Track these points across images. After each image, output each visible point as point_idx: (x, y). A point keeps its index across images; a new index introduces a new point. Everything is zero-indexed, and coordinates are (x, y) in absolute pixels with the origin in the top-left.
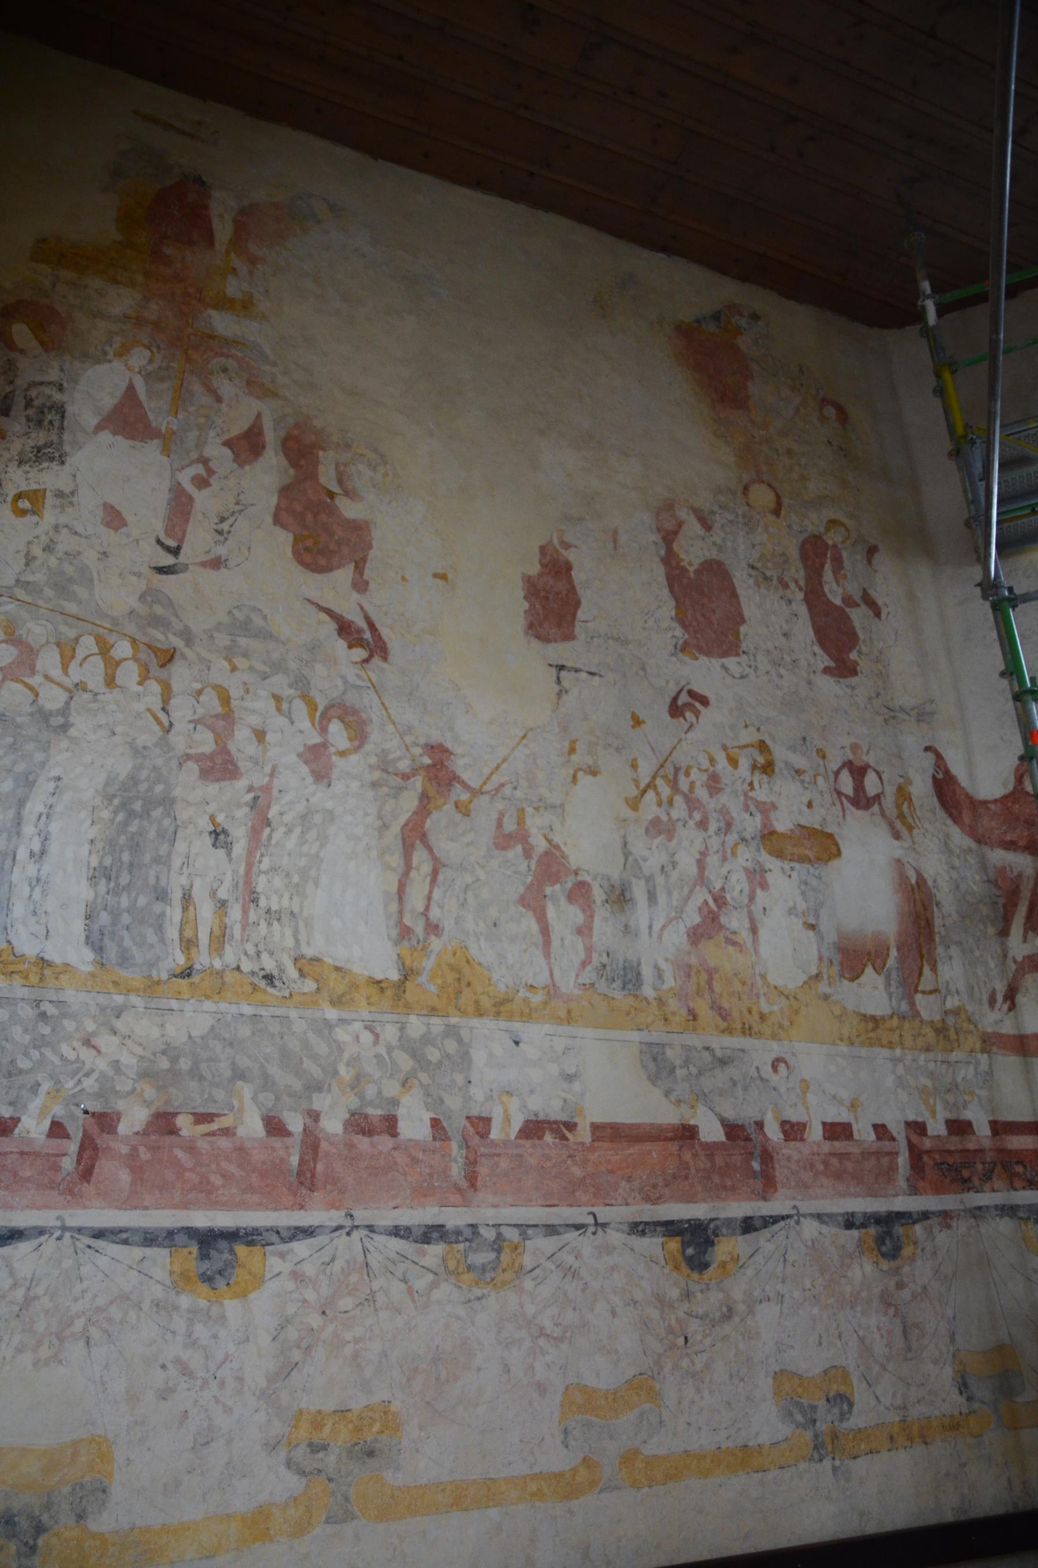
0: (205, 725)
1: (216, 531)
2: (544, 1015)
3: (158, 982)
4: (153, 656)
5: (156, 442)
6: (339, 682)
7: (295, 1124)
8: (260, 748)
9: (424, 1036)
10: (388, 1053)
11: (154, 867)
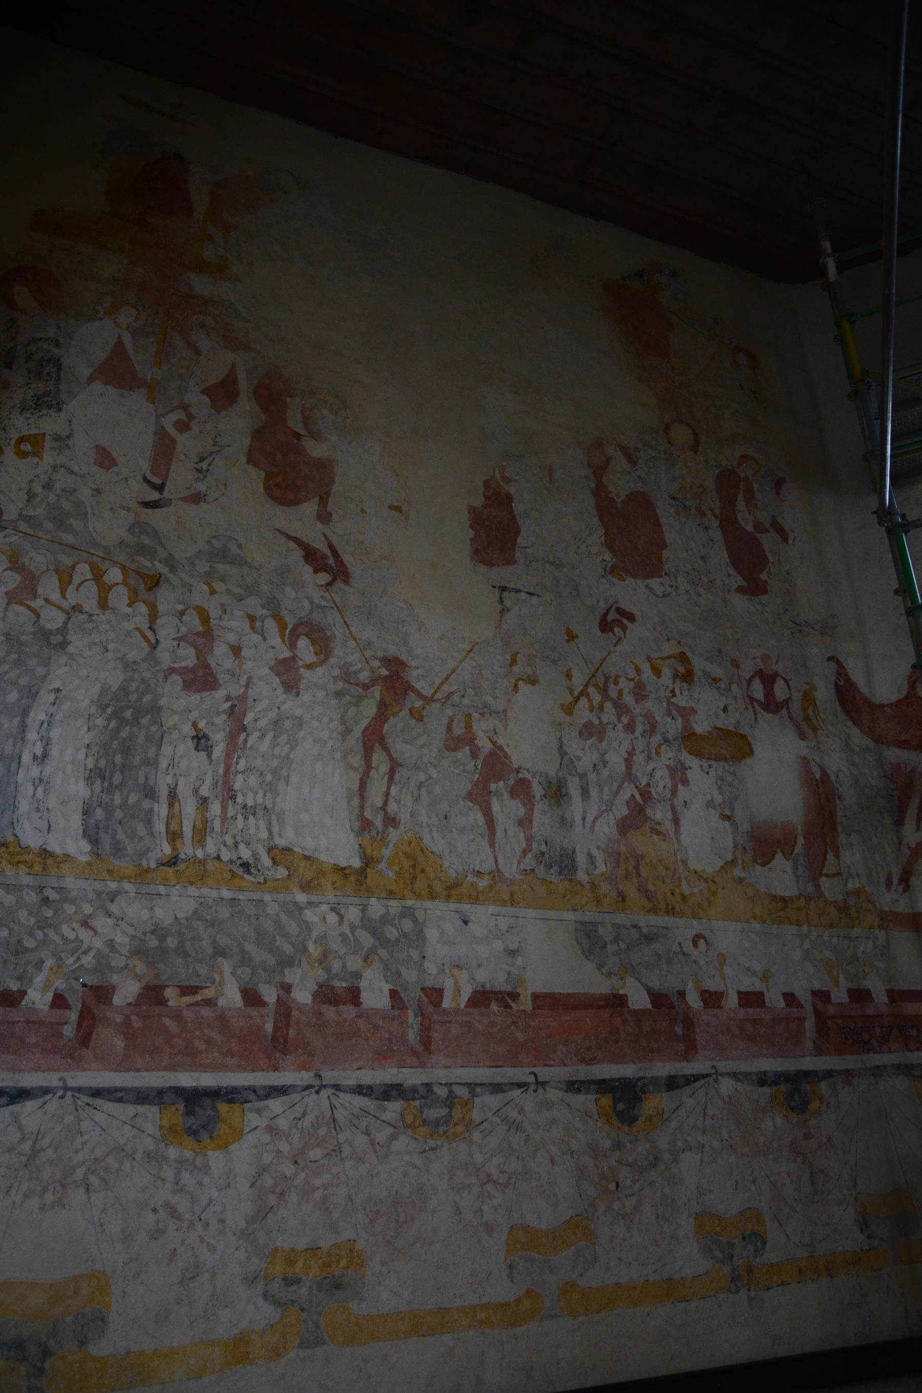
0: (187, 642)
1: (196, 469)
2: (490, 898)
3: (148, 870)
4: (141, 581)
5: (143, 391)
7: (270, 995)
8: (236, 662)
9: (383, 916)
10: (352, 932)
11: (143, 768)
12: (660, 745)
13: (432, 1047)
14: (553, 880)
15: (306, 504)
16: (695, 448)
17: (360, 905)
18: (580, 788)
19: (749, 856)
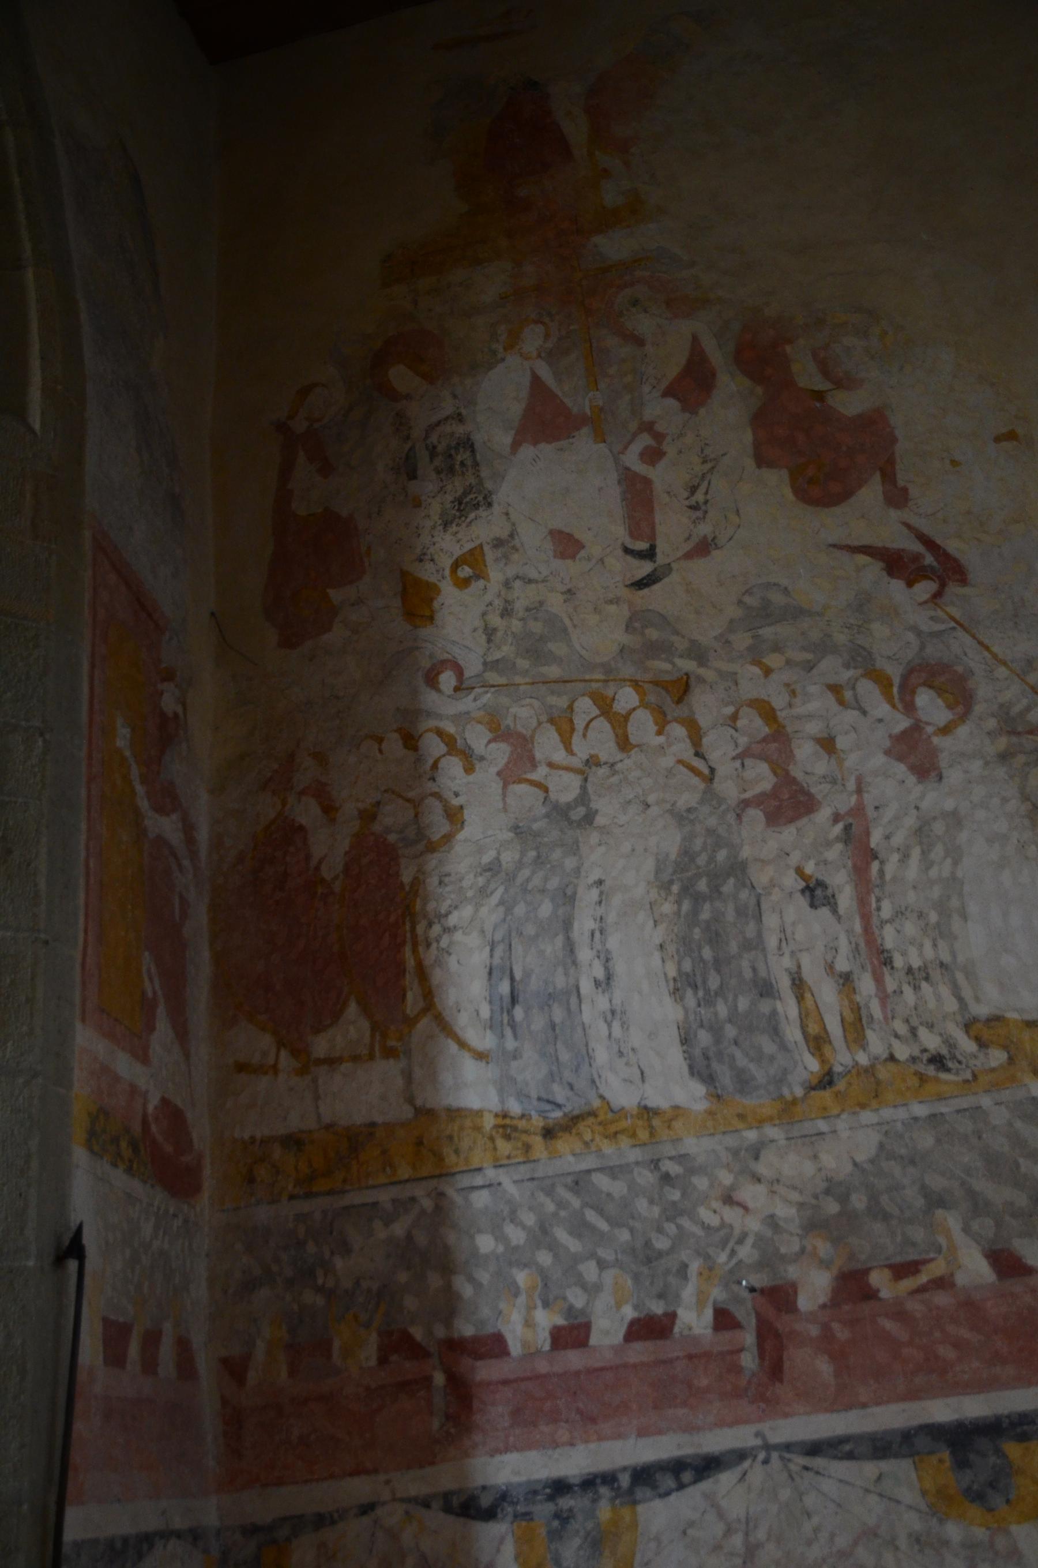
0: (753, 756)
1: (690, 507)
3: (794, 1102)
4: (664, 693)
5: (585, 430)
11: (745, 956)
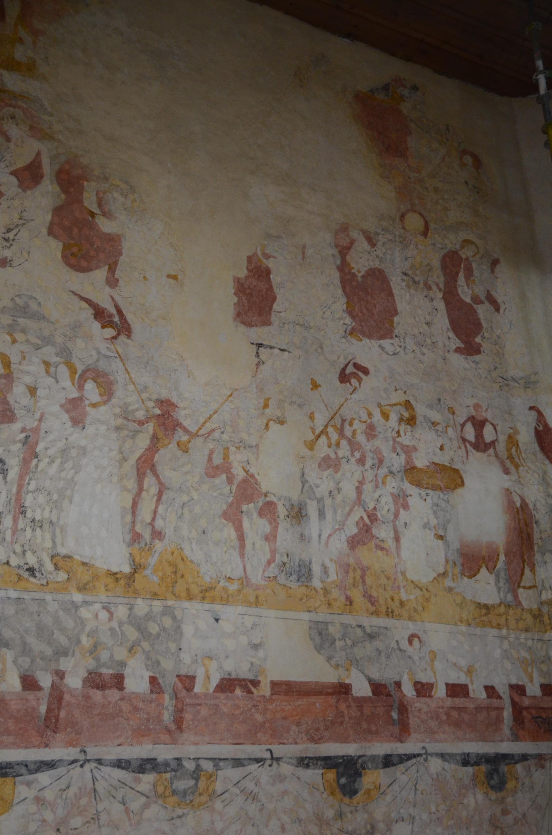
1: (4, 239)
2: (238, 600)
6: (94, 353)
9: (147, 614)
10: (119, 627)
12: (386, 476)
13: (184, 726)
14: (292, 586)
15: (97, 271)
16: (425, 234)
17: (127, 604)
18: (318, 510)
19: (458, 569)
